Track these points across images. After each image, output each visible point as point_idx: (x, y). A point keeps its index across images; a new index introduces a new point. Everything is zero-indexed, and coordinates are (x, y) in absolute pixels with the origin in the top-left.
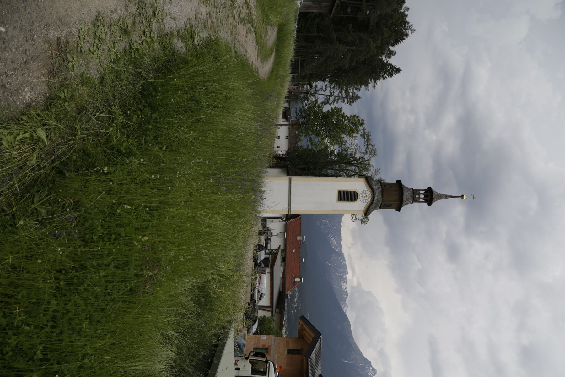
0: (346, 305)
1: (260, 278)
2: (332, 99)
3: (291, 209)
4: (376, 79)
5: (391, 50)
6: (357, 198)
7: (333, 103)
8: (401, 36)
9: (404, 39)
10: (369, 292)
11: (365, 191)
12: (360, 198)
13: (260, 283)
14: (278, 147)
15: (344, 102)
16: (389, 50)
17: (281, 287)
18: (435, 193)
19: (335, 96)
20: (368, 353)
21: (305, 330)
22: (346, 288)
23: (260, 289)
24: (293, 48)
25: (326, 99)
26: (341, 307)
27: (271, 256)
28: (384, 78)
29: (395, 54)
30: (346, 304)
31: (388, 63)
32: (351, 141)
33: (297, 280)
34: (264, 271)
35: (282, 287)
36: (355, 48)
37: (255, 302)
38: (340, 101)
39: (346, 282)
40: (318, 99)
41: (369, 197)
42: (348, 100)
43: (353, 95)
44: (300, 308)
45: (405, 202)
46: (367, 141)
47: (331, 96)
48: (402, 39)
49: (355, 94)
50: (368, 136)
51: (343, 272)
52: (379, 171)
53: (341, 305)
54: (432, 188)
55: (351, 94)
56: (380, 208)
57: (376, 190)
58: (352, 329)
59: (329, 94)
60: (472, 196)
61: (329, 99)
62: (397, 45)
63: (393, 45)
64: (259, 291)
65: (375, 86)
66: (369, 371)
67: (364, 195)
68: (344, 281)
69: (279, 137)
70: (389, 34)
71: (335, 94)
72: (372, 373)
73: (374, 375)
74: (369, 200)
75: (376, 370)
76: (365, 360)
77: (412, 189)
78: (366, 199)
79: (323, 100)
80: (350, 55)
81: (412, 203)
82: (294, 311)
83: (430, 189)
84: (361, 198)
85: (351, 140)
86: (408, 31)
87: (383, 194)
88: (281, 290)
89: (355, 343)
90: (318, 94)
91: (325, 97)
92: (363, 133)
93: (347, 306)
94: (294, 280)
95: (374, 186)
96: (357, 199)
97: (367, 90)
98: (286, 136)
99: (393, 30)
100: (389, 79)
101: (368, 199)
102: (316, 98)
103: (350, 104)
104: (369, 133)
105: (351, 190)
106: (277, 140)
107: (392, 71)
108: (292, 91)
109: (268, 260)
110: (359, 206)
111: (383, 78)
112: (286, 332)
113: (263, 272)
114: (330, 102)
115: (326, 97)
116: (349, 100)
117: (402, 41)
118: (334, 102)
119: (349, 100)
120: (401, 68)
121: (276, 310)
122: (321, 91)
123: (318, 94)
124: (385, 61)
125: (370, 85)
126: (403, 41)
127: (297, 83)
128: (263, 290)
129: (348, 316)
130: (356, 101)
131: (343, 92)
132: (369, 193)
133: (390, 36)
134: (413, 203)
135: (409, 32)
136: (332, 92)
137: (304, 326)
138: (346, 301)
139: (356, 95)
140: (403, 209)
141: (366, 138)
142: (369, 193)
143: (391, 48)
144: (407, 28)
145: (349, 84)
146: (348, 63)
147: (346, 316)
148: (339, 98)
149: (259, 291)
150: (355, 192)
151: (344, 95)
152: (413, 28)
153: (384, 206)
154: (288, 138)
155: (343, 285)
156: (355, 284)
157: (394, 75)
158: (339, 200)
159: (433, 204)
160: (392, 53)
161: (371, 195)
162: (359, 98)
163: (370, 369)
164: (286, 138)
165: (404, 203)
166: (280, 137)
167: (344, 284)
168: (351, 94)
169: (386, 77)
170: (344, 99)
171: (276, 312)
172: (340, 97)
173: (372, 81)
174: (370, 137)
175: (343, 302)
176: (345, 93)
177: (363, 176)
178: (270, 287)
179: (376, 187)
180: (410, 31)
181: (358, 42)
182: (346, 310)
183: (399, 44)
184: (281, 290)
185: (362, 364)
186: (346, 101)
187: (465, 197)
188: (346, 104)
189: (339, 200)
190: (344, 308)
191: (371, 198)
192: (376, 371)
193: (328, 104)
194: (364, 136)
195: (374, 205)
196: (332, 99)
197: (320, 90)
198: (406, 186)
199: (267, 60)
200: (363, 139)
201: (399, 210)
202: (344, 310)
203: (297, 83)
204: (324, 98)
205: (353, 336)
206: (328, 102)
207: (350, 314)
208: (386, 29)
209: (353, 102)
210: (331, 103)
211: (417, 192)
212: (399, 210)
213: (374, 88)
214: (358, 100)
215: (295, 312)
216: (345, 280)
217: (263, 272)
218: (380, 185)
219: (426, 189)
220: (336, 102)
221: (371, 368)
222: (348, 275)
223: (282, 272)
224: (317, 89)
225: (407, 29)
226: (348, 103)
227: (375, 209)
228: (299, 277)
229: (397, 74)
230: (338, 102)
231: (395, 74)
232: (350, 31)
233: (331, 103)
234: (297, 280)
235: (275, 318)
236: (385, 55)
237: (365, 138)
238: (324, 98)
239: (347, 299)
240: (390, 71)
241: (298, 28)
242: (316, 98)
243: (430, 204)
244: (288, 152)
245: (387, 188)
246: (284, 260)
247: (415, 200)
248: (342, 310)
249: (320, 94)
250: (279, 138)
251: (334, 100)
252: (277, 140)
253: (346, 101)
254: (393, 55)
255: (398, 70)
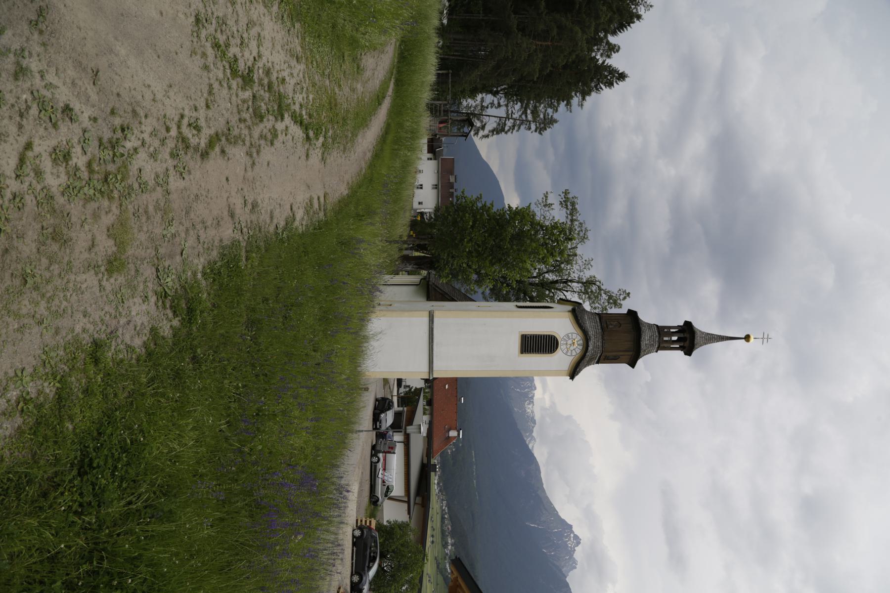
0: (533, 438)
1: (385, 460)
2: (509, 123)
3: (434, 369)
4: (585, 94)
5: (611, 44)
6: (557, 348)
7: (511, 131)
8: (629, 19)
9: (633, 22)
10: (569, 418)
11: (570, 335)
12: (562, 347)
13: (384, 469)
14: (420, 203)
15: (530, 129)
16: (608, 43)
17: (425, 455)
18: (698, 332)
19: (515, 120)
20: (567, 511)
21: (459, 586)
22: (533, 412)
23: (386, 478)
24: (431, 78)
25: (499, 124)
26: (525, 441)
27: (405, 409)
28: (598, 89)
29: (618, 51)
30: (533, 437)
31: (605, 64)
32: (542, 213)
33: (453, 433)
34: (392, 448)
35: (427, 456)
36: (549, 43)
37: (378, 500)
38: (522, 127)
39: (533, 402)
40: (485, 124)
41: (578, 345)
42: (536, 125)
43: (544, 117)
44: (461, 445)
45: (645, 351)
46: (571, 214)
47: (507, 118)
48: (630, 22)
49: (548, 115)
50: (573, 204)
51: (529, 387)
52: (592, 263)
53: (525, 439)
54: (694, 324)
55: (542, 116)
56: (598, 362)
57: (591, 333)
58: (543, 475)
59: (505, 116)
60: (766, 336)
61: (505, 124)
62: (621, 32)
63: (614, 33)
64: (384, 482)
65: (582, 105)
66: (569, 540)
67: (570, 342)
68: (530, 401)
69: (421, 187)
70: (609, 16)
71: (514, 116)
72: (573, 542)
73: (577, 546)
74: (578, 351)
75: (580, 537)
76: (563, 522)
77: (657, 326)
78: (572, 348)
79: (495, 125)
80: (540, 56)
81: (657, 352)
82: (451, 449)
83: (688, 325)
84: (563, 347)
85: (542, 211)
86: (639, 8)
87: (603, 339)
88: (425, 461)
89: (547, 498)
90: (486, 115)
91: (497, 120)
92: (564, 199)
93: (535, 439)
94: (447, 434)
95: (588, 324)
96: (557, 348)
97: (569, 112)
98: (433, 185)
99: (615, 10)
100: (606, 91)
101: (577, 349)
102: (482, 122)
103: (540, 133)
104: (575, 200)
105: (546, 334)
106: (418, 192)
107: (611, 78)
108: (437, 132)
109: (401, 416)
110: (562, 358)
111: (597, 89)
112: (438, 484)
113: (390, 450)
114: (507, 128)
115: (500, 120)
116: (538, 125)
117: (629, 25)
118: (513, 129)
119: (538, 125)
120: (626, 72)
121: (415, 499)
122: (492, 107)
123: (486, 115)
124: (600, 62)
125: (575, 101)
126: (631, 25)
127: (446, 118)
128: (390, 480)
129: (535, 455)
130: (550, 127)
131: (529, 112)
132: (578, 338)
133: (610, 21)
134: (659, 351)
135: (641, 10)
136: (510, 112)
137: (460, 580)
138: (532, 431)
139: (550, 117)
140: (640, 362)
141: (570, 207)
142: (579, 338)
143: (612, 39)
144: (639, 2)
145: (538, 99)
146: (537, 70)
147: (533, 455)
148: (522, 122)
149: (384, 482)
150: (552, 336)
151: (530, 117)
152: (648, 3)
153: (605, 358)
154: (436, 188)
155: (529, 408)
156: (547, 404)
157: (615, 84)
158: (522, 352)
159: (694, 353)
160: (613, 49)
161: (581, 342)
162: (556, 121)
163: (571, 537)
164: (433, 188)
165: (642, 353)
166: (424, 187)
167: (530, 406)
168: (542, 116)
169: (601, 88)
170: (530, 124)
171: (415, 503)
172: (523, 120)
173: (578, 95)
174: (577, 206)
175: (528, 434)
176: (532, 113)
177: (570, 301)
178: (405, 474)
179: (592, 327)
180: (643, 8)
181: (555, 32)
182: (533, 447)
183: (623, 30)
184: (425, 461)
185: (557, 529)
186: (533, 127)
187: (752, 340)
188: (534, 133)
189: (522, 352)
190: (529, 443)
191: (581, 347)
192: (581, 540)
193: (503, 133)
194: (567, 205)
195: (587, 359)
196: (509, 123)
197: (490, 105)
198: (646, 321)
199: (367, 125)
200: (565, 210)
201: (633, 364)
202: (530, 446)
203: (446, 118)
204: (496, 122)
205: (544, 486)
206: (503, 130)
207: (540, 452)
208: (605, 8)
209: (546, 129)
210: (509, 130)
211: (666, 330)
212: (633, 364)
213: (580, 108)
214: (553, 125)
215: (452, 452)
216: (531, 400)
217: (390, 450)
218: (598, 320)
219: (682, 324)
220: (516, 128)
221: (572, 535)
222: (535, 392)
223: (428, 422)
224: (485, 104)
225: (638, 5)
226: (536, 131)
227: (589, 364)
228: (455, 429)
229: (620, 83)
230: (519, 128)
231: (616, 82)
232: (542, 13)
233: (509, 130)
234: (453, 433)
235: (413, 525)
236: (601, 51)
237: (567, 209)
238: (496, 122)
239: (535, 429)
240: (609, 78)
241: (450, 5)
242: (482, 122)
243: (688, 353)
244: (437, 209)
245: (610, 326)
246: (430, 403)
247: (663, 346)
248: (527, 446)
249: (489, 116)
250: (421, 188)
251: (514, 126)
252: (418, 192)
253: (533, 127)
254: (614, 52)
255: (622, 76)
